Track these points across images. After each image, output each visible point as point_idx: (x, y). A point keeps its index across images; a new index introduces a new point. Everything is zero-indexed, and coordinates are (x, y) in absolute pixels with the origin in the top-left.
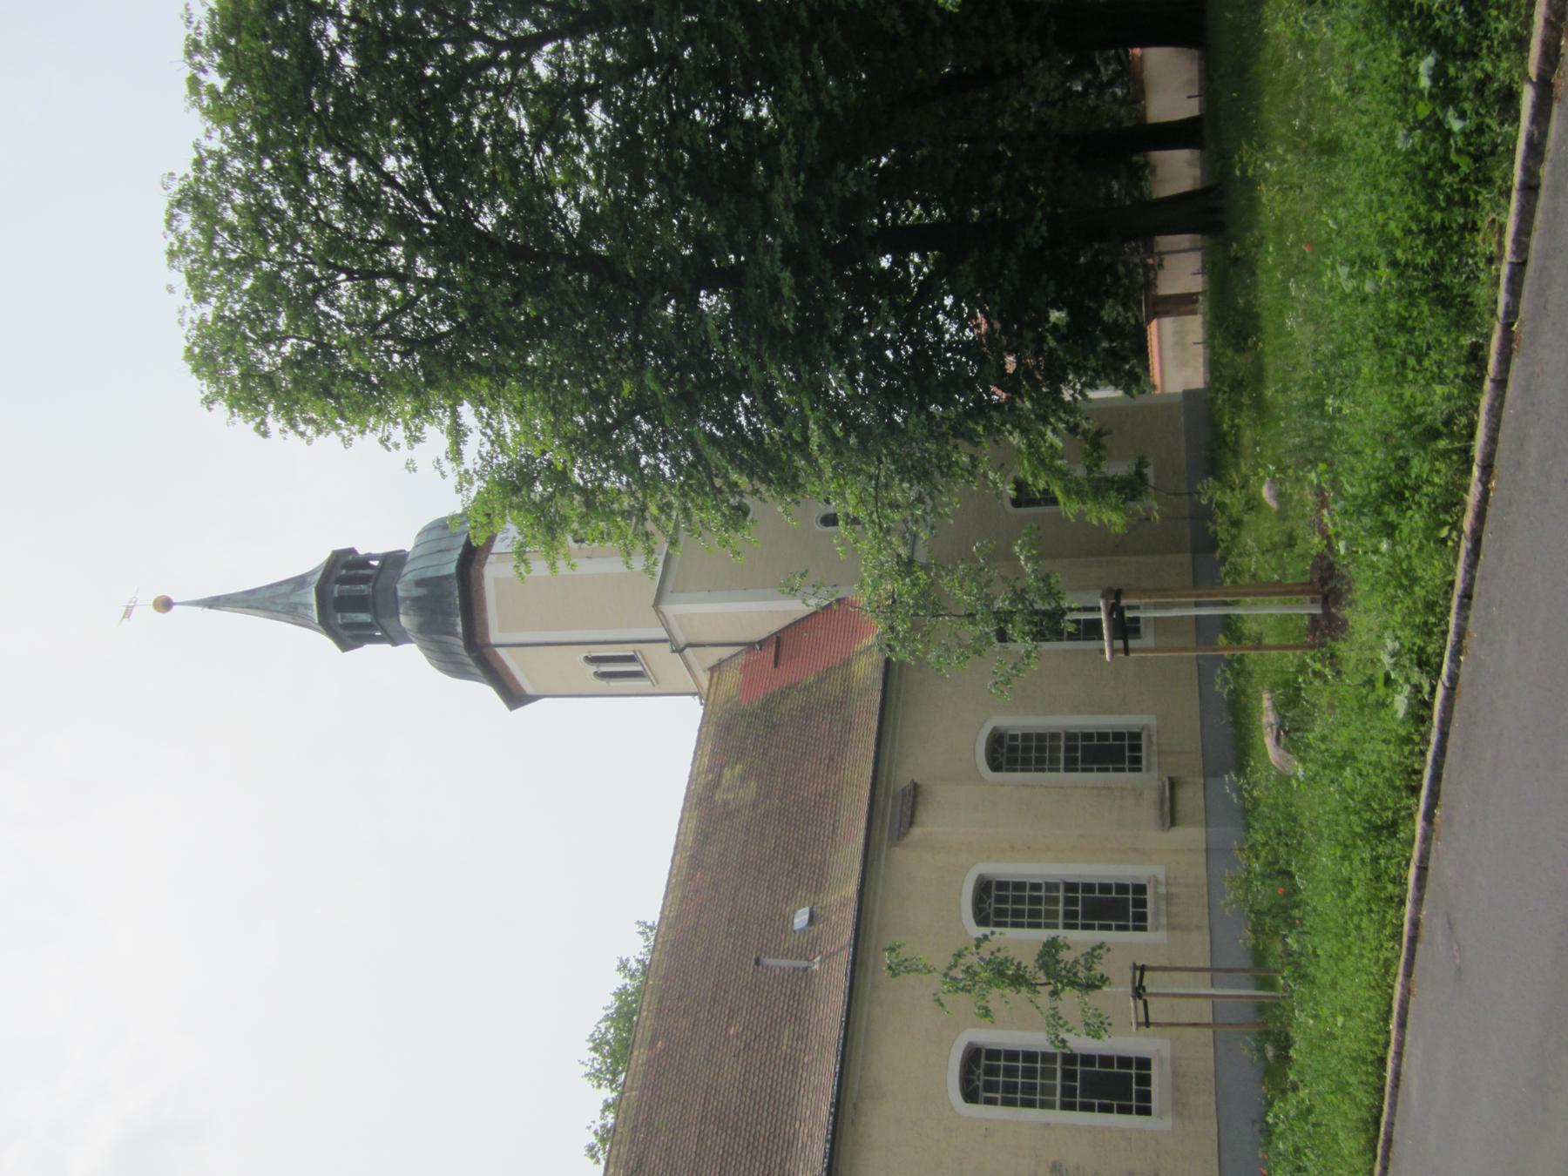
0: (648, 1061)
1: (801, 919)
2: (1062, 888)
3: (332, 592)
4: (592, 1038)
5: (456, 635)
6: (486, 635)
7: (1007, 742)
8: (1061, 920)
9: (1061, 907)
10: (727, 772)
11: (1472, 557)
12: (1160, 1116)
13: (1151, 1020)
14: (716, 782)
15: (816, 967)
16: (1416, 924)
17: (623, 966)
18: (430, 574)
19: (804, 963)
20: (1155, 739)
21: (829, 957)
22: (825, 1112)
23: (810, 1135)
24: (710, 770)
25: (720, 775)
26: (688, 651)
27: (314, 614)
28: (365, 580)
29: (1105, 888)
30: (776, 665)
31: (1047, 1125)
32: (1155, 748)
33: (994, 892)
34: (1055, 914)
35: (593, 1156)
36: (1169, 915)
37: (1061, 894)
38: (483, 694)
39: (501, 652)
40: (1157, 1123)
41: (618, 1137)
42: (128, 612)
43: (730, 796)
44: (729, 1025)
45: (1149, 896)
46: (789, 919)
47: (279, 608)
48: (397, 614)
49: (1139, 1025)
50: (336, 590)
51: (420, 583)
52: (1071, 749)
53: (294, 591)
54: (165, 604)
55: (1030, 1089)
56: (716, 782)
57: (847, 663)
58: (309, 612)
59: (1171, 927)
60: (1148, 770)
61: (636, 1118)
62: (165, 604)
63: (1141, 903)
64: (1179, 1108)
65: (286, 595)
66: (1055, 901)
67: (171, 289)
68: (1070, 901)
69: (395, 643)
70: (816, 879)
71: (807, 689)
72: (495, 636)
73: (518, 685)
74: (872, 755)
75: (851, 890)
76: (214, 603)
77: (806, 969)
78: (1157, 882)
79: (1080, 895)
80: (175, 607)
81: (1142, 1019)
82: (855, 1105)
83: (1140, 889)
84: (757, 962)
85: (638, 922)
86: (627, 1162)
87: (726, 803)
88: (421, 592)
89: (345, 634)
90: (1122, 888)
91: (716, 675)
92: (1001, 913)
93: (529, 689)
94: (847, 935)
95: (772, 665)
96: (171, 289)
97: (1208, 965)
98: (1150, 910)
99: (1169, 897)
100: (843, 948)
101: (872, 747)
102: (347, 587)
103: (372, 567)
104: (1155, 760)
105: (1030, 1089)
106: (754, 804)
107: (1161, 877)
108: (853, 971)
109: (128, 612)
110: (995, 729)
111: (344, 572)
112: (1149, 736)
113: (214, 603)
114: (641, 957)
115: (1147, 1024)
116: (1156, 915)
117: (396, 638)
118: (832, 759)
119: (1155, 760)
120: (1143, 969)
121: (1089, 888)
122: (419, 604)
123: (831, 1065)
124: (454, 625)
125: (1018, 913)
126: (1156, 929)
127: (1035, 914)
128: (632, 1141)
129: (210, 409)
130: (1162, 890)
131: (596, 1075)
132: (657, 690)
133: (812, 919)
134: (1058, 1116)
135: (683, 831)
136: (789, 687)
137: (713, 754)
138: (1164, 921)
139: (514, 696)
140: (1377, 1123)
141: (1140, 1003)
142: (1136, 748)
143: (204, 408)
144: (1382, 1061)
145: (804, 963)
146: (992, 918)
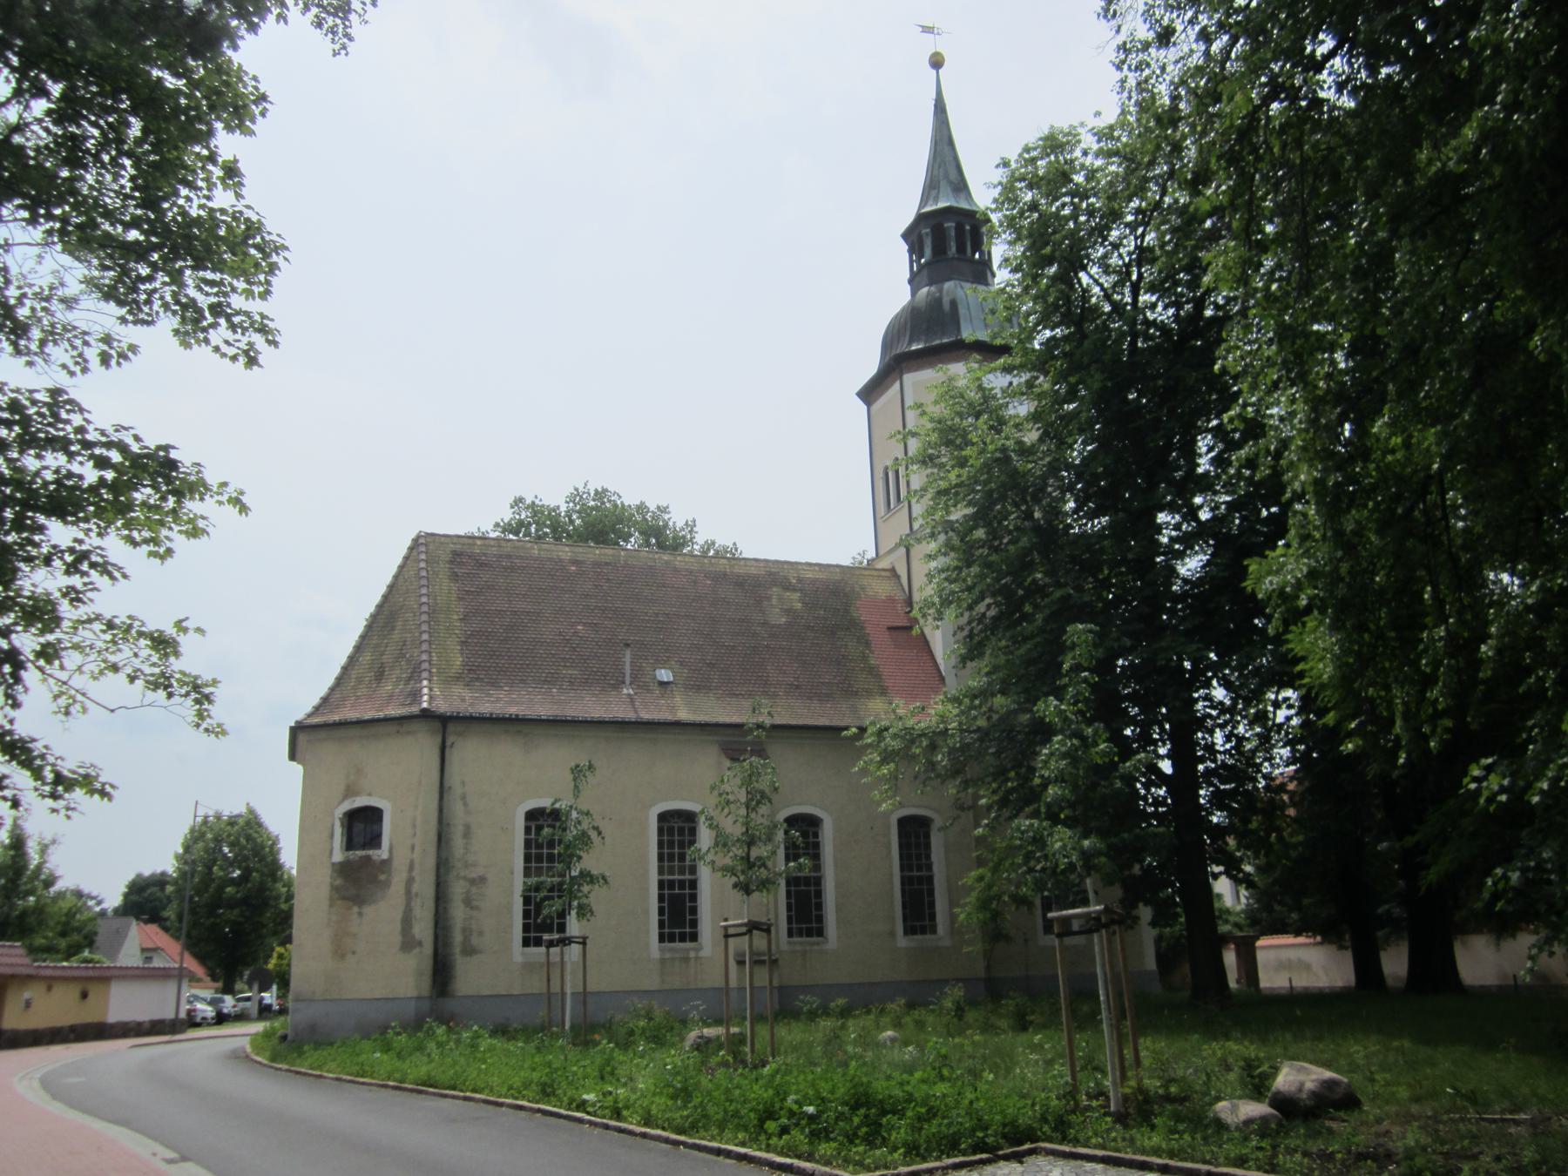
0: (561, 560)
1: (664, 675)
2: (692, 877)
3: (948, 221)
4: (605, 491)
5: (910, 343)
6: (910, 370)
7: (811, 830)
8: (666, 877)
9: (676, 877)
10: (796, 596)
11: (147, 1026)
12: (523, 954)
13: (731, 940)
14: (788, 587)
15: (625, 691)
16: (501, 1105)
17: (664, 510)
18: (962, 311)
19: (628, 682)
20: (816, 947)
21: (632, 701)
22: (513, 710)
23: (498, 700)
24: (800, 580)
25: (795, 590)
26: (903, 550)
27: (928, 209)
28: (961, 249)
29: (694, 910)
30: (891, 629)
31: (512, 873)
32: (808, 948)
33: (687, 825)
34: (671, 872)
35: (515, 502)
36: (673, 959)
37: (687, 877)
38: (871, 366)
39: (897, 386)
40: (518, 952)
41: (503, 544)
42: (928, 30)
43: (774, 602)
44: (584, 625)
45: (688, 945)
46: (664, 664)
47: (936, 172)
48: (930, 284)
49: (726, 928)
50: (950, 225)
51: (954, 304)
52: (920, 880)
53: (950, 183)
54: (937, 62)
55: (539, 858)
56: (788, 587)
57: (883, 692)
58: (931, 202)
59: (663, 961)
60: (789, 943)
61: (517, 557)
62: (937, 62)
63: (683, 939)
64: (528, 967)
65: (946, 176)
66: (682, 872)
67: (1098, 114)
68: (682, 884)
69: (910, 281)
70: (697, 684)
71: (865, 658)
72: (910, 378)
73: (875, 401)
74: (794, 722)
75: (684, 715)
76: (940, 108)
77: (624, 682)
78: (697, 950)
79: (687, 891)
80: (934, 72)
81: (731, 931)
82: (519, 732)
83: (694, 937)
84: (627, 645)
85: (694, 521)
86: (485, 554)
87: (769, 598)
88: (946, 306)
89: (914, 237)
90: (694, 923)
91: (888, 574)
92: (671, 831)
93: (876, 407)
94: (645, 715)
95: (890, 624)
96: (1098, 114)
97: (588, 990)
98: (678, 945)
99: (686, 960)
100: (636, 712)
101: (800, 722)
102: (953, 233)
103: (974, 254)
104: (798, 948)
105: (539, 858)
106: (765, 624)
107: (703, 954)
108: (617, 722)
109: (928, 30)
110: (821, 820)
111: (968, 228)
112: (818, 944)
113: (940, 108)
114: (671, 524)
115: (727, 936)
116: (671, 950)
117: (914, 281)
118: (797, 687)
119: (798, 948)
120: (584, 943)
121: (694, 898)
122: (935, 303)
123: (543, 710)
124: (918, 341)
125: (671, 844)
126: (661, 950)
127: (671, 857)
128: (501, 556)
129: (998, 166)
130: (692, 954)
131: (575, 497)
132: (879, 521)
133: (662, 684)
134: (519, 882)
135: (749, 563)
136: (868, 644)
137: (814, 581)
138: (668, 955)
139: (869, 393)
140: (431, 1086)
141: (744, 929)
142: (809, 933)
143: (998, 161)
144: (454, 1088)
145: (628, 682)
146: (665, 826)
